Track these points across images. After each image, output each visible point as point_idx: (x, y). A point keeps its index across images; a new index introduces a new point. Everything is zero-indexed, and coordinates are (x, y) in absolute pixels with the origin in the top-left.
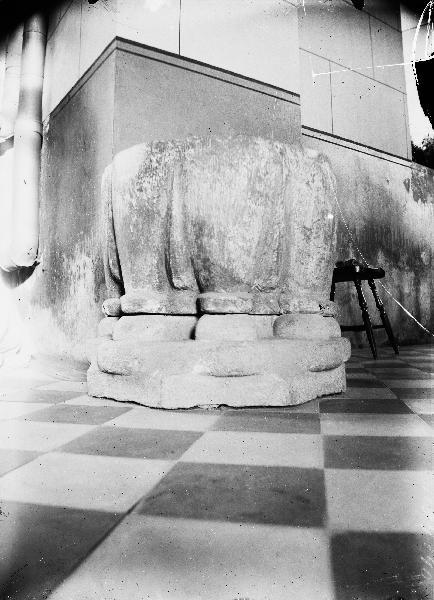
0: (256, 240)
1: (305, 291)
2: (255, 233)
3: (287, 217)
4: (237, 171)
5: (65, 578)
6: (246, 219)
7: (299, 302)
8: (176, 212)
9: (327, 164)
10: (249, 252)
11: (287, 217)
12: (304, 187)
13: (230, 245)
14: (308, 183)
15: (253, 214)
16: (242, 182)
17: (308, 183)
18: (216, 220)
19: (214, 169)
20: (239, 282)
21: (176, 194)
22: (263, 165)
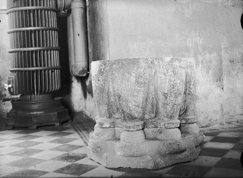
0: (141, 101)
1: (167, 119)
2: (140, 98)
3: (156, 90)
4: (131, 75)
5: (217, 149)
6: (135, 94)
7: (164, 124)
8: (111, 90)
9: (108, 126)
10: (138, 106)
11: (156, 90)
12: (163, 76)
13: (130, 104)
14: (165, 74)
15: (139, 91)
16: (133, 79)
17: (165, 74)
18: (125, 94)
19: (122, 75)
20: (136, 118)
21: (111, 83)
22: (142, 70)
